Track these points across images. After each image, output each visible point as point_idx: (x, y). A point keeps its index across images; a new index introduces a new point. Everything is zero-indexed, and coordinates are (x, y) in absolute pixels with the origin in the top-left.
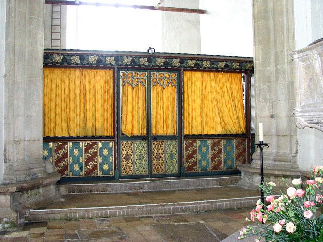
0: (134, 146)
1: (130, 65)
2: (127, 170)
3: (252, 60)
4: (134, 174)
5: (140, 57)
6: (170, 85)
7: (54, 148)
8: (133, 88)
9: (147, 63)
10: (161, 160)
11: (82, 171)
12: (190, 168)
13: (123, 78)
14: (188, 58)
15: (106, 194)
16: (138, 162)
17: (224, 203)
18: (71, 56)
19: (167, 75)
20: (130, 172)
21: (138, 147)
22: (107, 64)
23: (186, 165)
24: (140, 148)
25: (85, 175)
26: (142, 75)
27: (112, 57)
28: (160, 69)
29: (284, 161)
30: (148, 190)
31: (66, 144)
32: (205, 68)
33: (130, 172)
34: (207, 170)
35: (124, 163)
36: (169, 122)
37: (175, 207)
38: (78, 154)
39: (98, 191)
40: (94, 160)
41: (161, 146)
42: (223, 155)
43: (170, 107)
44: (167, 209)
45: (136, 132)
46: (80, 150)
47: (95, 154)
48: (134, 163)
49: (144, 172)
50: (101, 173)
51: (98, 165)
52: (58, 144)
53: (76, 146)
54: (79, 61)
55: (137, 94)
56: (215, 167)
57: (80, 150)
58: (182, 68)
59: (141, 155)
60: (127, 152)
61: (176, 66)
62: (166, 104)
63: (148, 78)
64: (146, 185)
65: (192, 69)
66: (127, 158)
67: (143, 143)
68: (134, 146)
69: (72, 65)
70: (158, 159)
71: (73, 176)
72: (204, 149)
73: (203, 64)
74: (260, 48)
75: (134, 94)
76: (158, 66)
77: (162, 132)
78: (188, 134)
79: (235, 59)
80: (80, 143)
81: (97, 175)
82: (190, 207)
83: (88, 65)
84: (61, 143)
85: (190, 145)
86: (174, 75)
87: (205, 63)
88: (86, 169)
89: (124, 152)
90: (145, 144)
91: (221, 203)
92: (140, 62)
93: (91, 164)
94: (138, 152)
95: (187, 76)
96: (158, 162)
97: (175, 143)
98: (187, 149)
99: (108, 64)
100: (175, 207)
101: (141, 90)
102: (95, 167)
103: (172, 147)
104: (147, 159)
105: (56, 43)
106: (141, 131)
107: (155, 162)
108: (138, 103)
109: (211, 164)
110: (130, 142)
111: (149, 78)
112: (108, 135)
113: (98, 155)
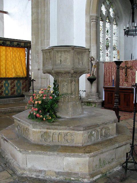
34: (8, 95)
42: (16, 88)
56: (12, 94)
57: (8, 84)
72: (7, 85)
109: (10, 92)
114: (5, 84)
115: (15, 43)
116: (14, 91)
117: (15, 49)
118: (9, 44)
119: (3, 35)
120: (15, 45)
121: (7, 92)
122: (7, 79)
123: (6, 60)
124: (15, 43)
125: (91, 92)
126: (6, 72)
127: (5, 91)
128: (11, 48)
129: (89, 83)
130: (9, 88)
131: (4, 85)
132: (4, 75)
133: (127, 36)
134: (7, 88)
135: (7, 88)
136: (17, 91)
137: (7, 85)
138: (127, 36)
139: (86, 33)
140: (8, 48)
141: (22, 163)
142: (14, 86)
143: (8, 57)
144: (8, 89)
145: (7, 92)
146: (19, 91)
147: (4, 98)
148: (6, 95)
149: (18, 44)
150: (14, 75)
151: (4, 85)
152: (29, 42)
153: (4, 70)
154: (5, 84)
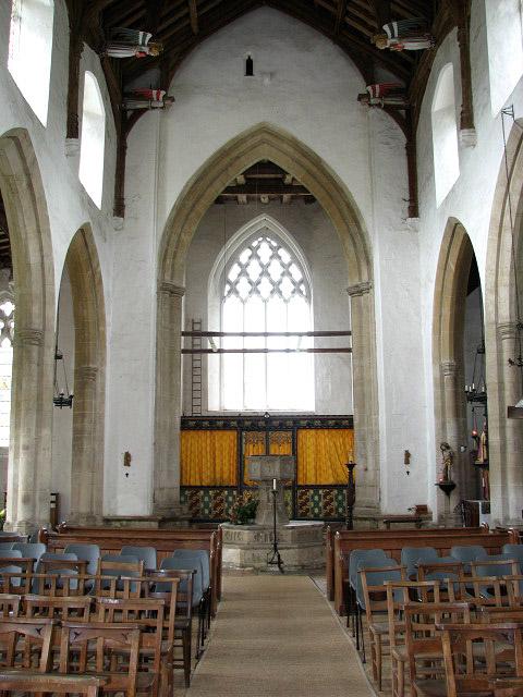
23: (300, 501)
26: (261, 435)
42: (335, 504)
47: (307, 500)
53: (316, 493)
56: (328, 514)
72: (316, 498)
86: (290, 434)
93: (218, 508)
95: (302, 434)
109: (324, 511)
116: (331, 510)
122: (316, 487)
123: (317, 452)
124: (192, 423)
125: (448, 512)
126: (316, 474)
127: (203, 510)
128: (326, 432)
129: (442, 493)
130: (321, 504)
132: (314, 479)
134: (316, 504)
135: (316, 504)
137: (316, 498)
139: (436, 398)
140: (319, 432)
142: (331, 500)
145: (316, 511)
149: (336, 424)
150: (331, 481)
152: (350, 419)
153: (313, 472)
154: (336, 496)
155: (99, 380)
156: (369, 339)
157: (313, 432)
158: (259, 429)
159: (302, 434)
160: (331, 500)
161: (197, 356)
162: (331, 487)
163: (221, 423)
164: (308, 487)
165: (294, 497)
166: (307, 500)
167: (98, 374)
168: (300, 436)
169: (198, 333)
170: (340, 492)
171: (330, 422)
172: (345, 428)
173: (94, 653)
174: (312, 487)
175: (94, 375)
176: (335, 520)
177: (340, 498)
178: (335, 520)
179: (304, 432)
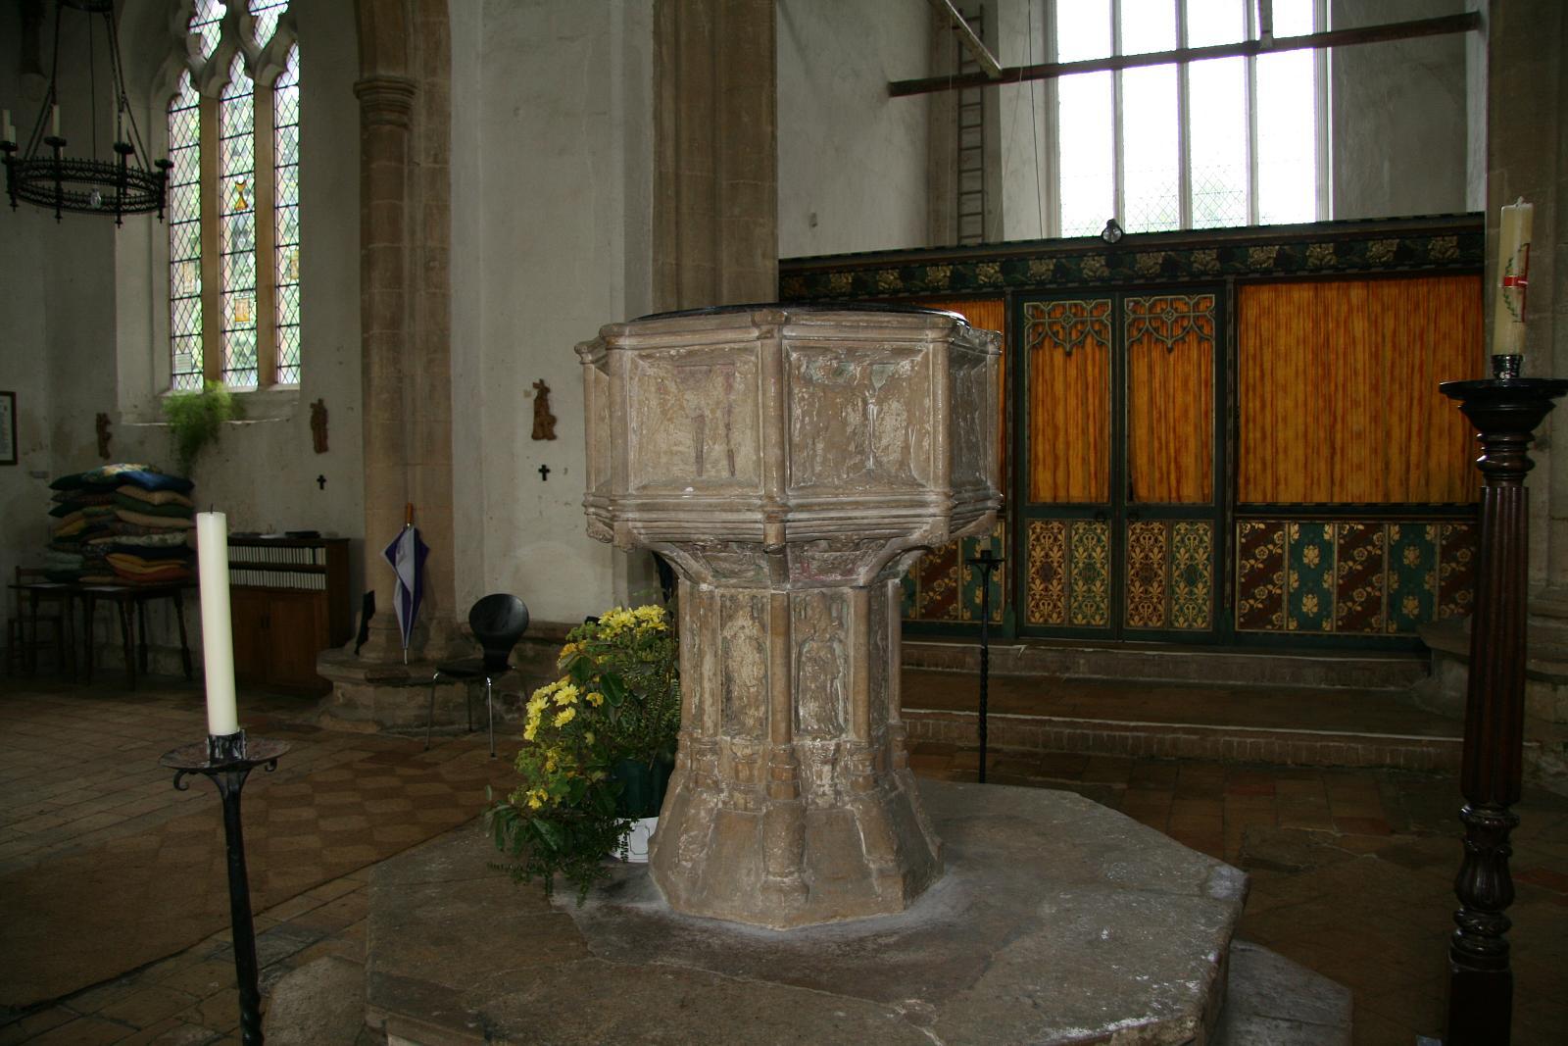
0: (1069, 538)
1: (1051, 282)
2: (1046, 609)
3: (1474, 222)
4: (1066, 624)
5: (879, 267)
6: (1192, 339)
7: (1439, 544)
8: (1068, 354)
9: (1106, 273)
10: (1155, 585)
11: (914, 602)
12: (1256, 618)
13: (1035, 325)
14: (1246, 240)
15: (960, 675)
16: (1080, 587)
17: (1249, 740)
18: (877, 270)
19: (1184, 303)
20: (1055, 616)
21: (1081, 540)
22: (981, 287)
23: (1244, 606)
24: (1092, 544)
25: (923, 616)
26: (1097, 311)
27: (994, 262)
28: (1151, 287)
29: (1557, 618)
30: (1088, 676)
31: (1279, 527)
32: (1319, 269)
33: (1055, 616)
34: (1319, 627)
35: (1038, 586)
36: (1189, 461)
37: (1079, 731)
38: (1316, 561)
39: (937, 666)
40: (948, 576)
41: (1156, 540)
42: (1387, 581)
43: (1192, 413)
44: (1053, 736)
45: (1077, 492)
46: (1427, 549)
47: (1274, 562)
48: (1069, 589)
49: (1097, 617)
50: (1293, 625)
51: (1285, 598)
52: (1454, 529)
53: (1311, 536)
54: (900, 284)
55: (1082, 372)
56: (1352, 621)
57: (1325, 549)
58: (1230, 278)
59: (1090, 565)
60: (1090, 556)
61: (1205, 273)
62: (1179, 400)
63: (1113, 319)
64: (1082, 661)
65: (1266, 278)
66: (1047, 573)
67: (1098, 527)
68: (1069, 538)
69: (881, 296)
70: (1147, 581)
71: (1399, 630)
72: (1311, 555)
73: (1306, 259)
74: (1506, 176)
75: (1073, 372)
76: (1143, 276)
77: (1165, 495)
78: (1324, 500)
79: (1442, 224)
80: (1428, 528)
81: (956, 617)
82: (1127, 738)
83: (928, 293)
84: (1465, 528)
85: (1264, 537)
86: (1208, 303)
87: (1436, 244)
88: (925, 599)
89: (1038, 554)
90: (1103, 531)
91: (1236, 740)
92: (1081, 270)
93: (940, 585)
94: (1080, 554)
95: (1258, 303)
96: (1146, 591)
97: (1204, 530)
98: (1247, 552)
99: (985, 285)
100: (1079, 731)
101: (1095, 362)
102: (1274, 602)
103: (1195, 543)
104: (1108, 581)
105: (972, 228)
106: (1093, 490)
107: (1137, 589)
108: (1085, 402)
109: (1338, 609)
110: (1056, 524)
111: (1118, 314)
112: (1374, 501)
113: (1386, 566)
114: (1296, 550)
115: (890, 278)
116: (1372, 605)
117: (1390, 291)
118: (1453, 253)
119: (1003, 237)
120: (1383, 264)
121: (1310, 604)
122: (1311, 514)
127: (1296, 598)
130: (1329, 581)
131: (1386, 557)
133: (58, 217)
135: (1311, 580)
136: (1391, 605)
137: (1311, 555)
138: (58, 217)
140: (1331, 293)
141: (680, 1038)
142: (1373, 565)
143: (1033, 373)
144: (1320, 580)
146: (1411, 606)
147: (1282, 643)
148: (1300, 627)
149: (1402, 254)
151: (1386, 557)
154: (1396, 550)
155: (421, 122)
156: (869, 643)
157: (1302, 294)
158: (1086, 290)
159: (965, 123)
160: (1373, 565)
161: (971, 95)
162: (1376, 513)
163: (846, 280)
164: (1277, 513)
165: (1221, 552)
166: (1274, 562)
167: (419, 103)
168: (1251, 312)
169: (1419, 505)
170: (1412, 535)
171: (1375, 249)
172: (1442, 270)
173: (823, 746)
174: (1294, 511)
175: (405, 109)
176: (1384, 646)
177: (1410, 556)
178: (1384, 646)
179: (1265, 295)
